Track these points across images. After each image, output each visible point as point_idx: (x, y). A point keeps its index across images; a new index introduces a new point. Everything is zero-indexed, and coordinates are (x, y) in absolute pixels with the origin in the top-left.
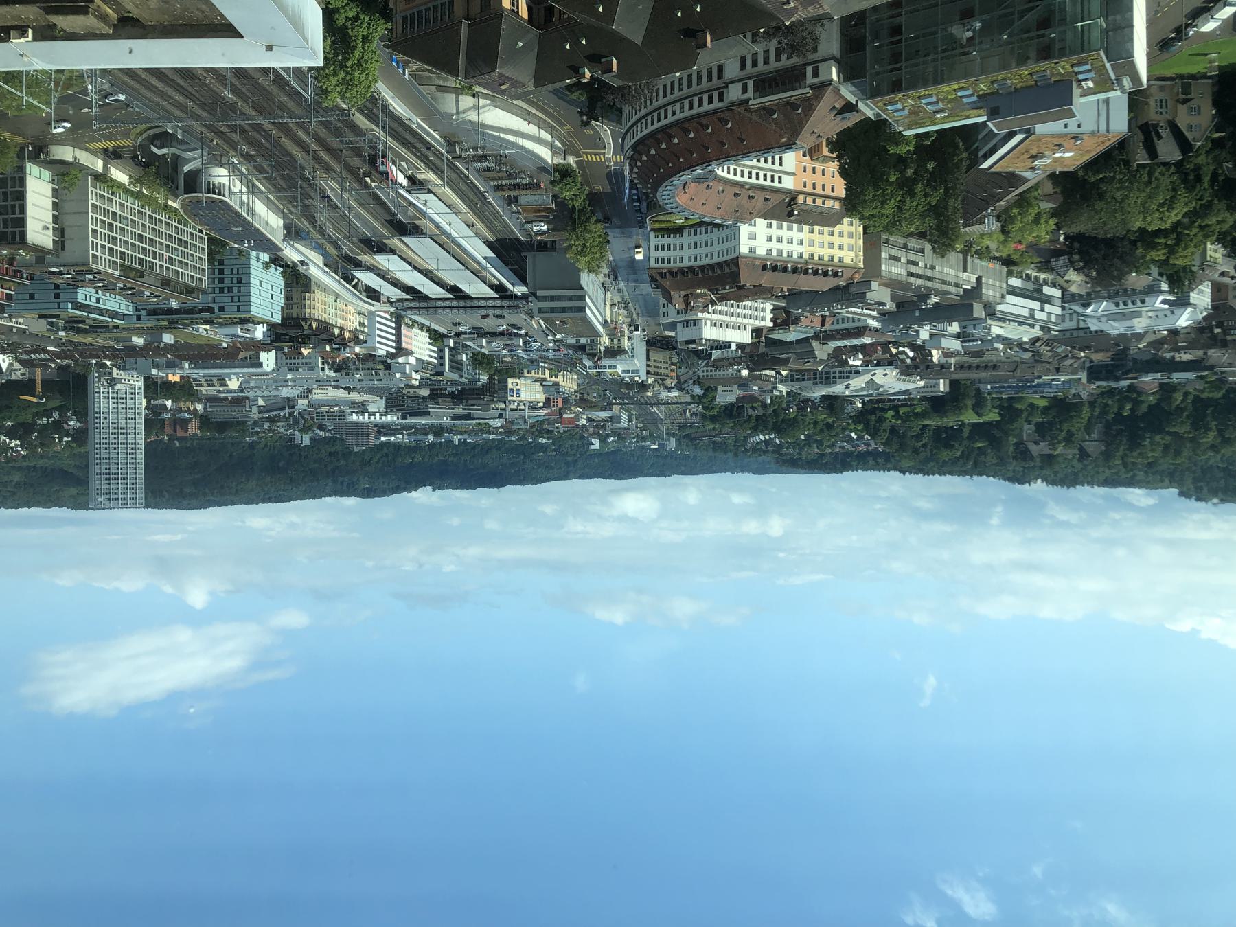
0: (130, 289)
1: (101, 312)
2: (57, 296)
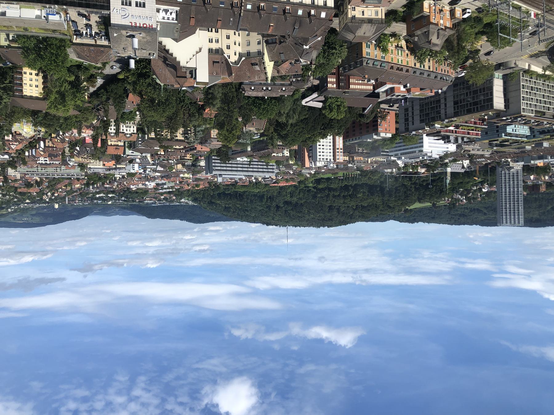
0: (537, 122)
1: (517, 136)
2: (497, 131)
